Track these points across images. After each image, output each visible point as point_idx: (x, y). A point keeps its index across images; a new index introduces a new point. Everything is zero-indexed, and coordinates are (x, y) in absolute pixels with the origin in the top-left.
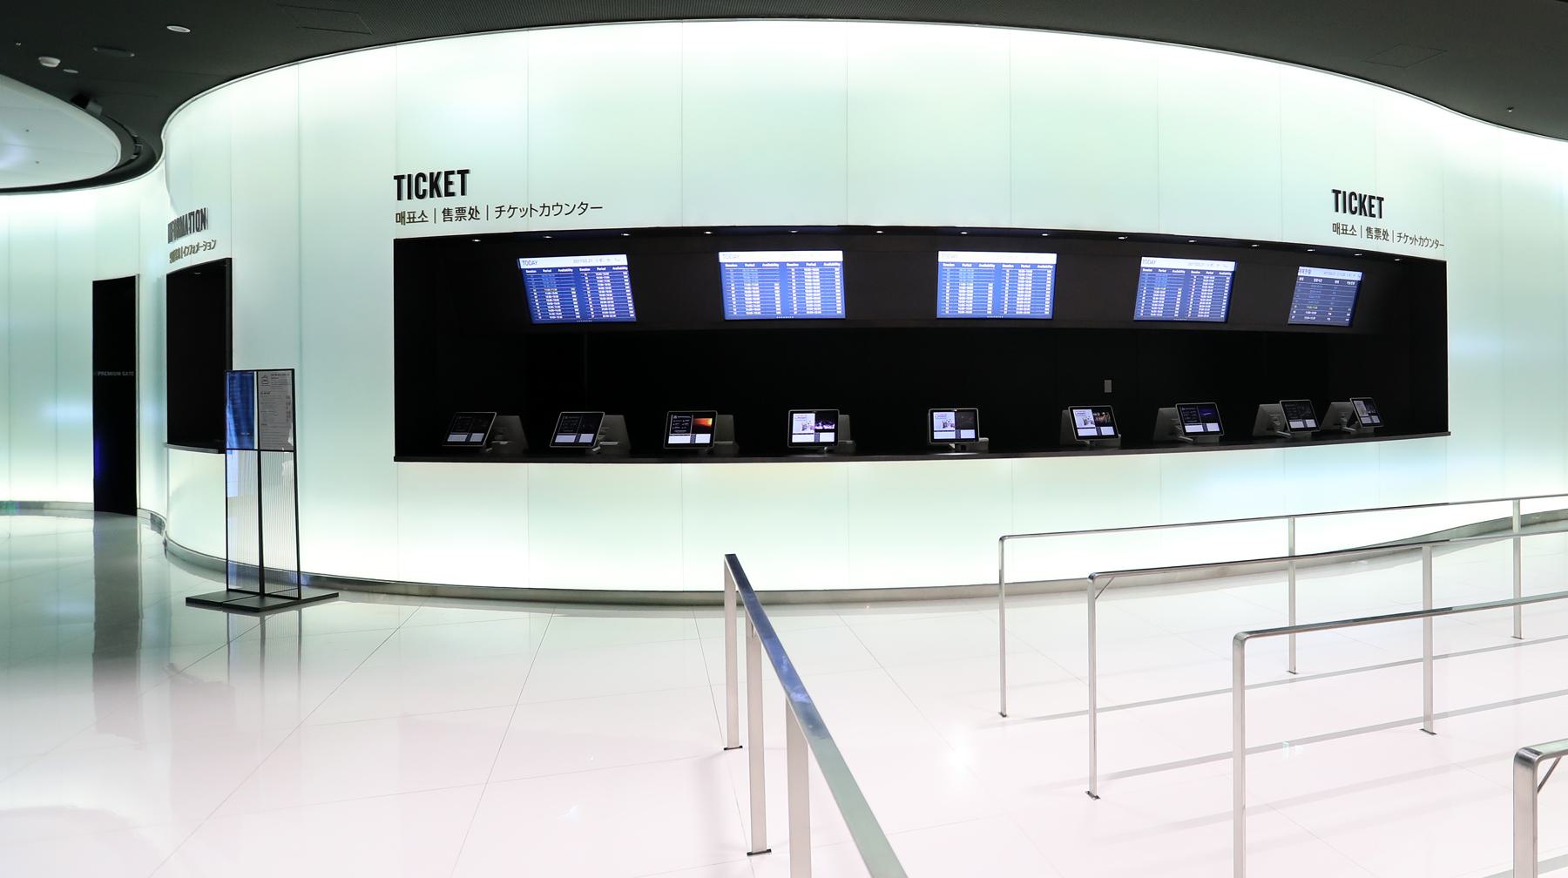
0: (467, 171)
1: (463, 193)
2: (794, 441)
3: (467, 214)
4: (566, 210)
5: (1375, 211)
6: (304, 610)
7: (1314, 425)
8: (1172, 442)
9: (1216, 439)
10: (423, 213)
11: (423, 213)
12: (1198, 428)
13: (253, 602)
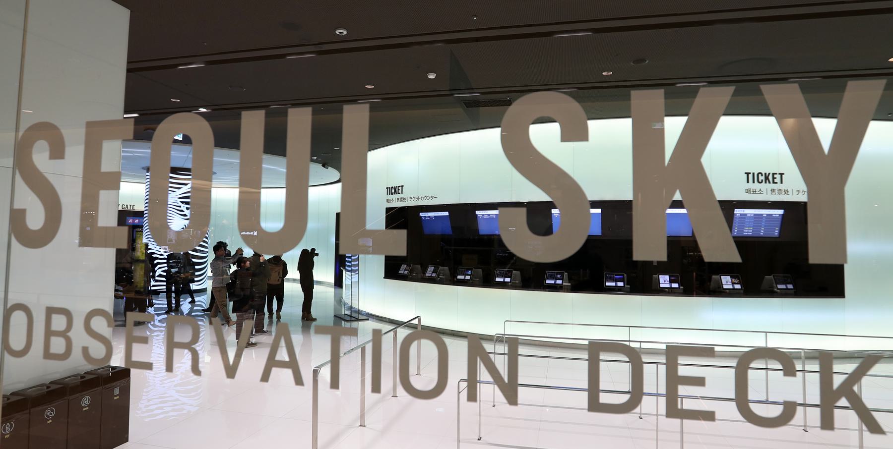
0: (783, 174)
1: (782, 183)
2: (547, 282)
3: (783, 192)
4: (428, 198)
5: (400, 191)
6: (359, 322)
7: (740, 288)
8: (771, 293)
9: (792, 292)
10: (760, 190)
11: (760, 190)
12: (783, 287)
13: (348, 318)
